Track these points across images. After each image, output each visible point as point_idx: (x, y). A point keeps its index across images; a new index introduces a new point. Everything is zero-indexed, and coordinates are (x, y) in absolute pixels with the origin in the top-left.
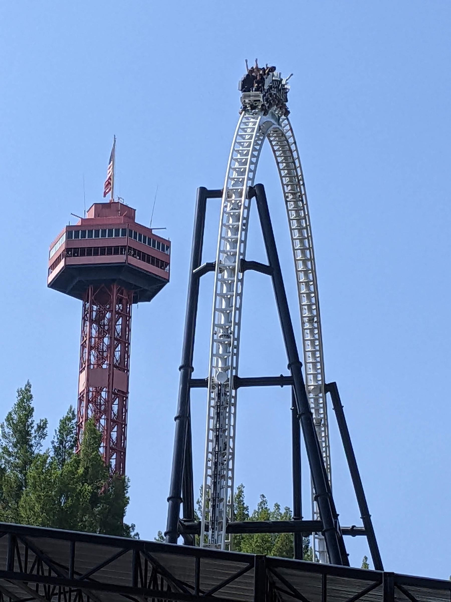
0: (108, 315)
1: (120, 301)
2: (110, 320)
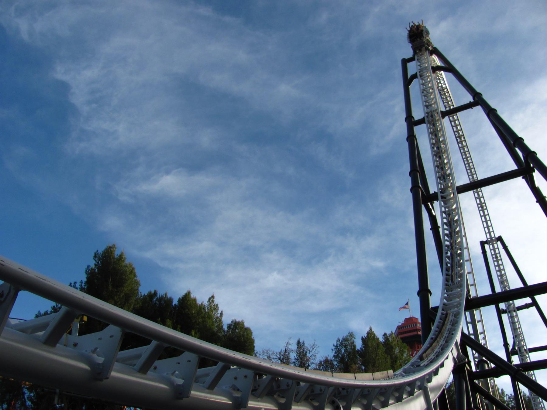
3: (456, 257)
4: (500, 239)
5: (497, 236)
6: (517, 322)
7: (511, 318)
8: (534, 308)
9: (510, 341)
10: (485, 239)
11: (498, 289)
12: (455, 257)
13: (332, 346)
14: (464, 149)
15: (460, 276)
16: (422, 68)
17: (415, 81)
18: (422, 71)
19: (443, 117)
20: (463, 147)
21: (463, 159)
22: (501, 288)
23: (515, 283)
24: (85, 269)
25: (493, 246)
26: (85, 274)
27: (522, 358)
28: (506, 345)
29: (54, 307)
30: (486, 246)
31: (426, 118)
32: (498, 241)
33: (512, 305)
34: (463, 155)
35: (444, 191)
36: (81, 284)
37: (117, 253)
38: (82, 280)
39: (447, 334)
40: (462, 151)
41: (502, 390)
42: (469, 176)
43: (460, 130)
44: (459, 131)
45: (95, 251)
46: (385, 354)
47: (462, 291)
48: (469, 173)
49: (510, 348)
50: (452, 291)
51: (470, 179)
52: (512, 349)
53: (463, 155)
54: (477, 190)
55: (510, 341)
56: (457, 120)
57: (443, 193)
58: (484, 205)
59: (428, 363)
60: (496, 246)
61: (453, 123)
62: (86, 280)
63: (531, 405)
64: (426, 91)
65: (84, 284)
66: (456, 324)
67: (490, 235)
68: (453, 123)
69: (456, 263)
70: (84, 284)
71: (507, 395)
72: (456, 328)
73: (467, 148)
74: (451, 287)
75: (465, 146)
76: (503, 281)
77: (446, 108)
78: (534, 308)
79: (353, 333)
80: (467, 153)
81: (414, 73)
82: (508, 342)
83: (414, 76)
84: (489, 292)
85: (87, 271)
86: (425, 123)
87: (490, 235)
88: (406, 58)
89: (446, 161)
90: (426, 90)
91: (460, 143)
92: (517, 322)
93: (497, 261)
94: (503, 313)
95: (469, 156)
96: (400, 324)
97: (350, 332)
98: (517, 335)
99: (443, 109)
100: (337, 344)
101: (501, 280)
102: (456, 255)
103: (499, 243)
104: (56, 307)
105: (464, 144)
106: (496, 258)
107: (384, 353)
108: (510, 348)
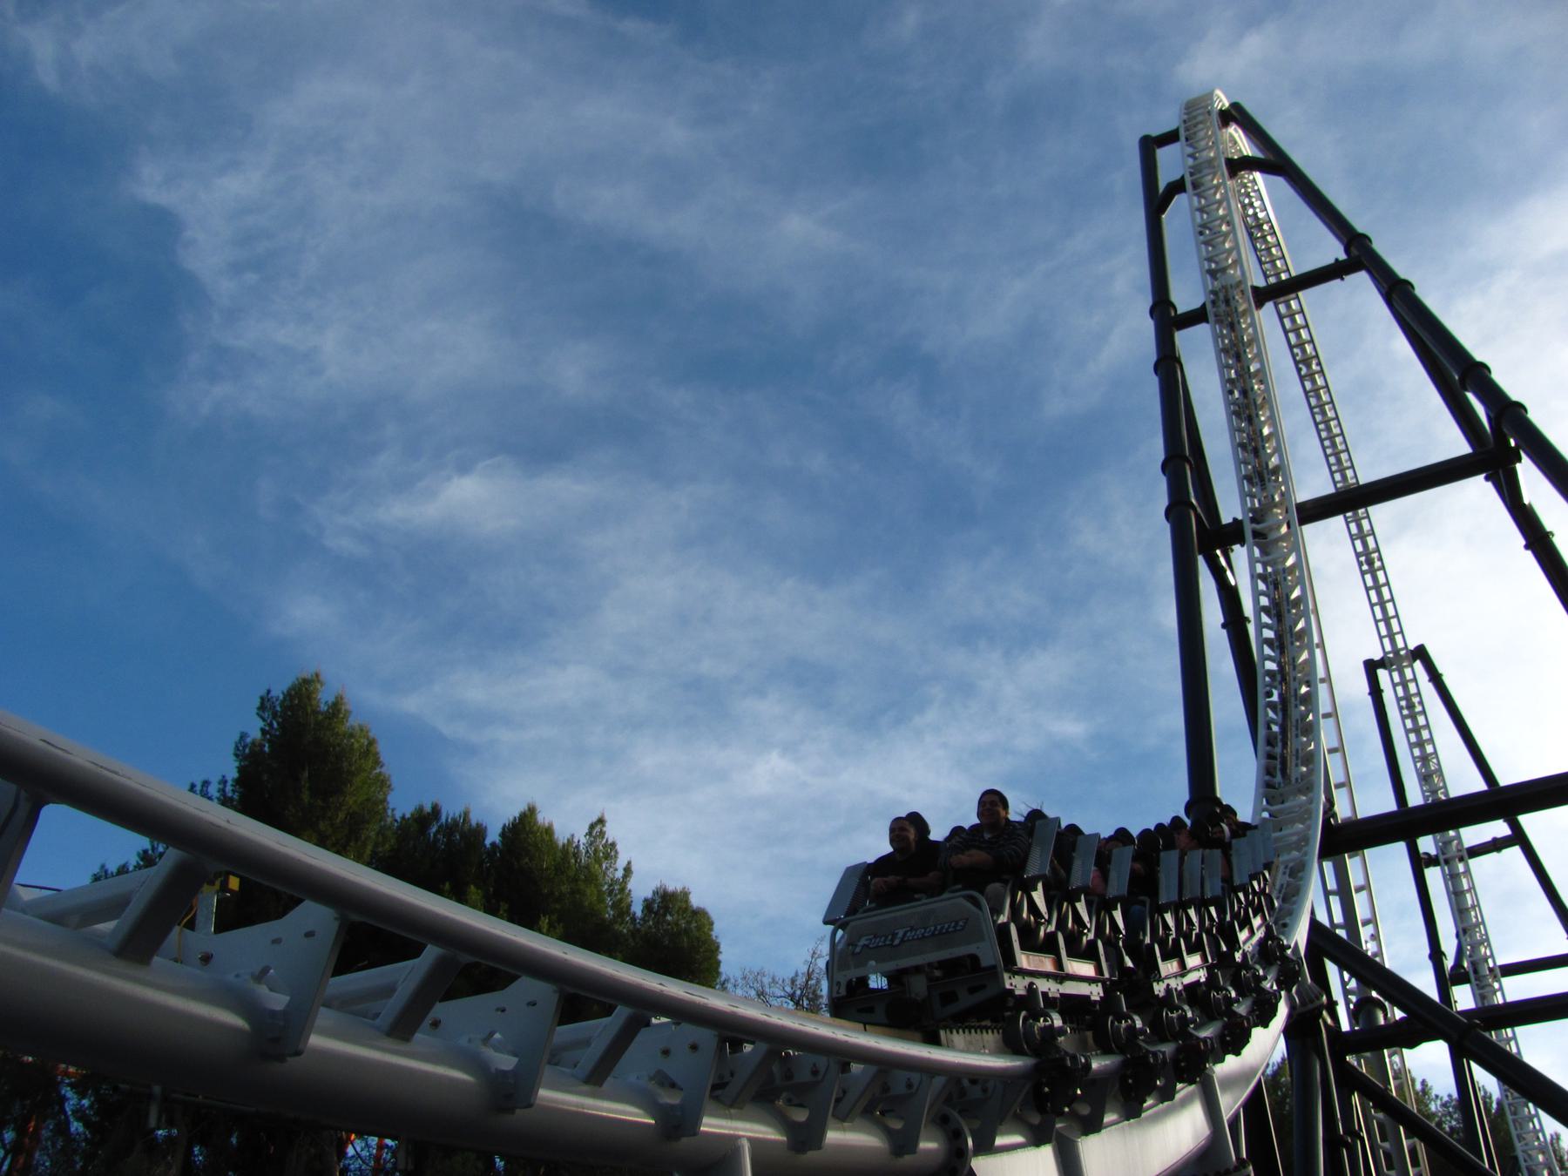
4: (1420, 653)
5: (1411, 647)
6: (1469, 890)
7: (1452, 879)
8: (1516, 851)
9: (1449, 945)
10: (1377, 655)
11: (1415, 797)
12: (1293, 705)
17: (1180, 202)
18: (1200, 172)
20: (1316, 391)
23: (1463, 780)
24: (233, 746)
25: (1402, 675)
26: (234, 758)
28: (1436, 954)
29: (145, 852)
30: (1382, 674)
31: (1209, 307)
32: (1415, 661)
35: (1262, 516)
36: (221, 786)
37: (324, 697)
38: (224, 777)
40: (1313, 401)
42: (1332, 473)
43: (1308, 342)
45: (263, 692)
48: (1328, 447)
49: (1449, 963)
50: (1283, 803)
51: (1335, 483)
52: (1452, 968)
53: (1316, 413)
54: (1356, 514)
55: (1449, 945)
57: (1258, 523)
58: (1375, 555)
60: (1408, 673)
62: (236, 775)
64: (1210, 229)
65: (232, 785)
67: (1393, 642)
69: (1294, 723)
70: (232, 785)
71: (1437, 1096)
74: (1280, 790)
75: (1323, 388)
76: (1429, 774)
77: (1266, 277)
78: (1516, 851)
81: (1176, 177)
83: (1177, 187)
84: (1390, 805)
85: (238, 749)
86: (1207, 322)
87: (1393, 642)
88: (1155, 132)
90: (1209, 225)
91: (1307, 378)
92: (1469, 890)
93: (1413, 717)
94: (1427, 866)
95: (1334, 416)
98: (1467, 926)
99: (1260, 282)
103: (1418, 665)
104: (150, 852)
105: (1320, 381)
106: (1410, 707)
108: (1449, 963)
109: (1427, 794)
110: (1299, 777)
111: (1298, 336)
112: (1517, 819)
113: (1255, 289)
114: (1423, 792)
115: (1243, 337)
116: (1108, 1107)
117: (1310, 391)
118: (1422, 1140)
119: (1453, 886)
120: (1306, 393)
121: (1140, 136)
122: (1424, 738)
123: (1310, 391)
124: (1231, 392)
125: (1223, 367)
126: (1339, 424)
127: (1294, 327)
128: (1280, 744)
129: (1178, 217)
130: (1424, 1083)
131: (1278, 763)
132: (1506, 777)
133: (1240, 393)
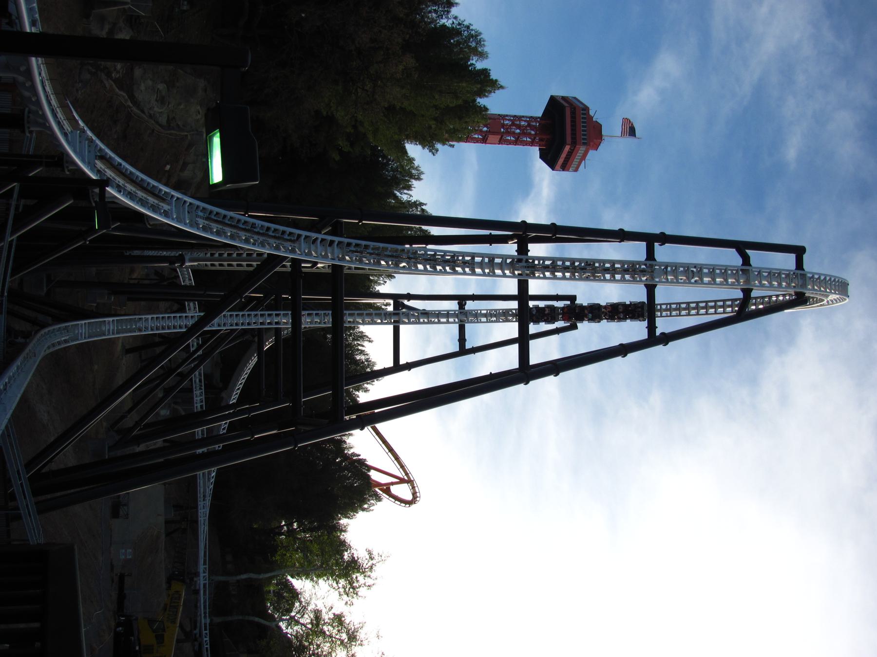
0: (533, 132)
1: (541, 140)
2: (530, 134)
3: (245, 235)
7: (447, 314)
12: (276, 241)
13: (470, 23)
14: (675, 310)
15: (219, 233)
16: (807, 279)
17: (738, 261)
19: (743, 290)
20: (670, 310)
21: (670, 304)
22: (498, 310)
27: (383, 314)
28: (410, 297)
31: (802, 272)
33: (407, 321)
34: (667, 306)
35: (340, 248)
39: (119, 182)
40: (674, 306)
41: (394, 277)
43: (698, 312)
44: (724, 308)
46: (445, 106)
47: (197, 228)
49: (406, 302)
50: (188, 212)
51: (661, 305)
53: (667, 306)
56: (724, 310)
57: (321, 242)
59: (66, 130)
61: (713, 304)
63: (321, 310)
64: (794, 278)
66: (141, 203)
68: (721, 303)
71: (386, 282)
72: (136, 202)
73: (675, 315)
74: (194, 212)
78: (456, 348)
79: (487, 59)
80: (678, 312)
81: (753, 262)
82: (411, 301)
83: (746, 260)
84: (532, 292)
86: (742, 265)
88: (805, 256)
89: (439, 268)
95: (672, 315)
96: (591, 113)
97: (488, 55)
98: (427, 316)
99: (754, 294)
100: (472, 30)
101: (510, 313)
102: (249, 236)
105: (683, 313)
107: (446, 105)
108: (406, 302)
109: (479, 311)
110: (240, 235)
111: (712, 307)
112: (517, 343)
113: (750, 290)
114: (499, 310)
115: (637, 275)
116: (25, 31)
117: (670, 306)
118: (254, 270)
119: (443, 314)
120: (680, 304)
121: (805, 246)
122: (449, 319)
123: (670, 306)
124: (695, 267)
125: (622, 262)
126: (667, 316)
127: (681, 309)
128: (244, 227)
129: (731, 258)
130: (394, 277)
131: (220, 219)
132: (532, 343)
133: (643, 268)
